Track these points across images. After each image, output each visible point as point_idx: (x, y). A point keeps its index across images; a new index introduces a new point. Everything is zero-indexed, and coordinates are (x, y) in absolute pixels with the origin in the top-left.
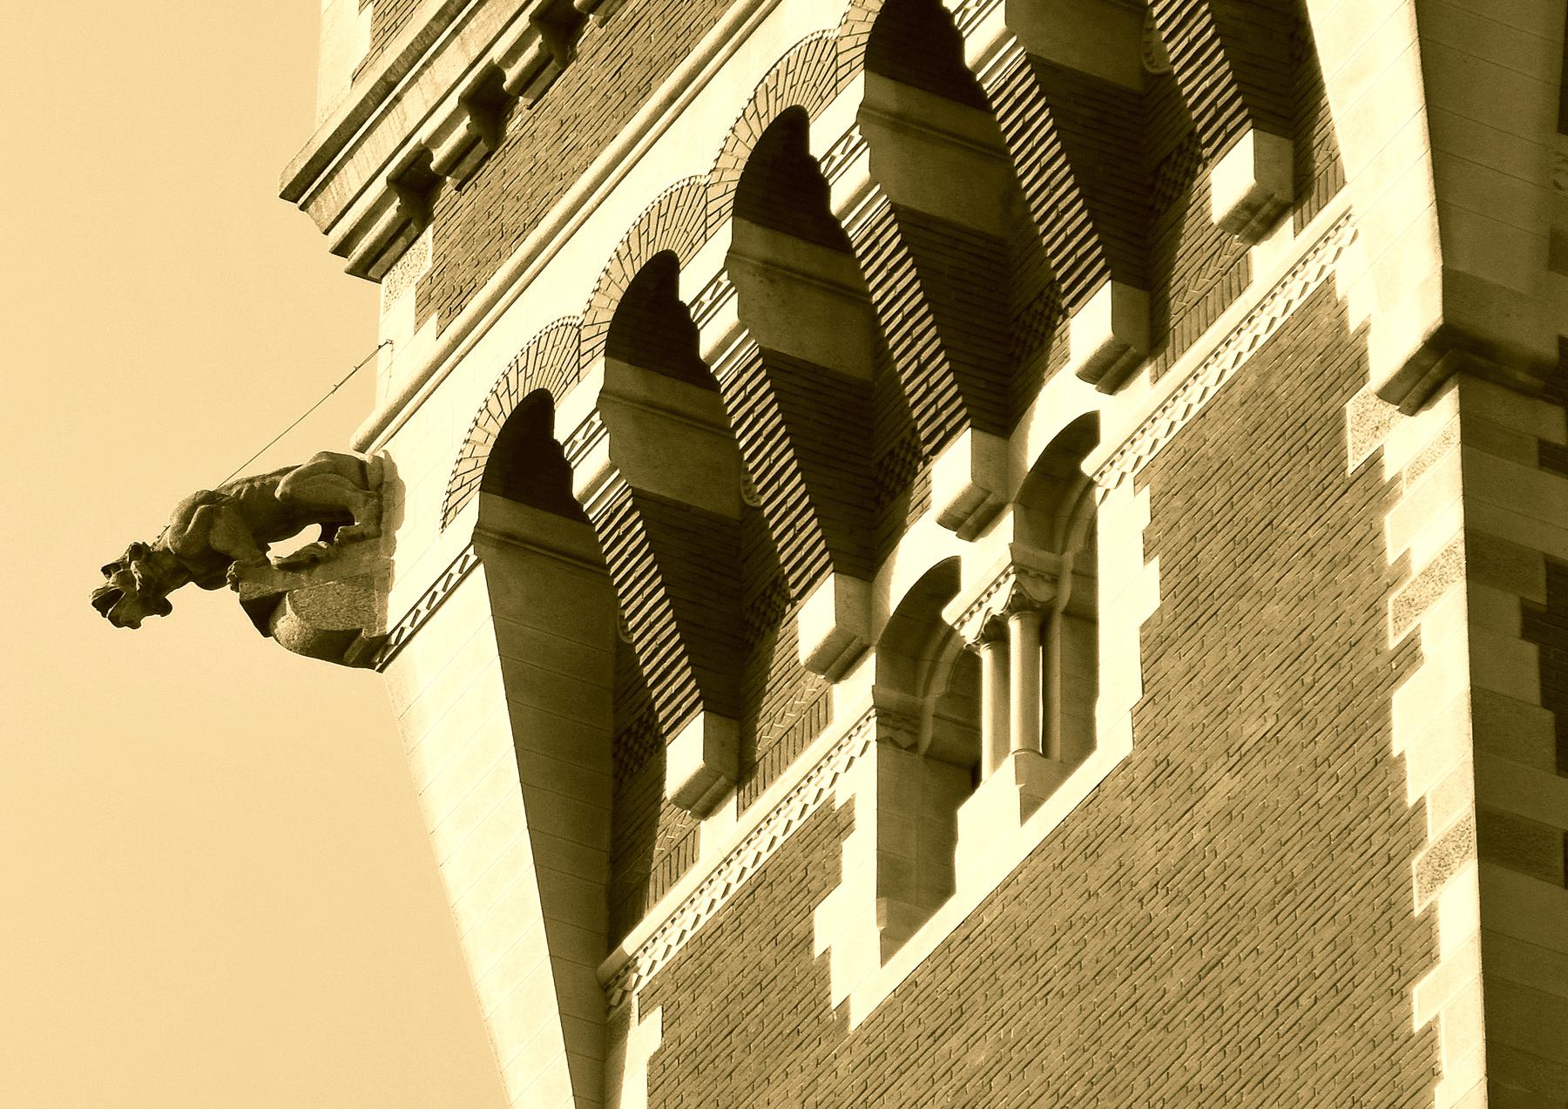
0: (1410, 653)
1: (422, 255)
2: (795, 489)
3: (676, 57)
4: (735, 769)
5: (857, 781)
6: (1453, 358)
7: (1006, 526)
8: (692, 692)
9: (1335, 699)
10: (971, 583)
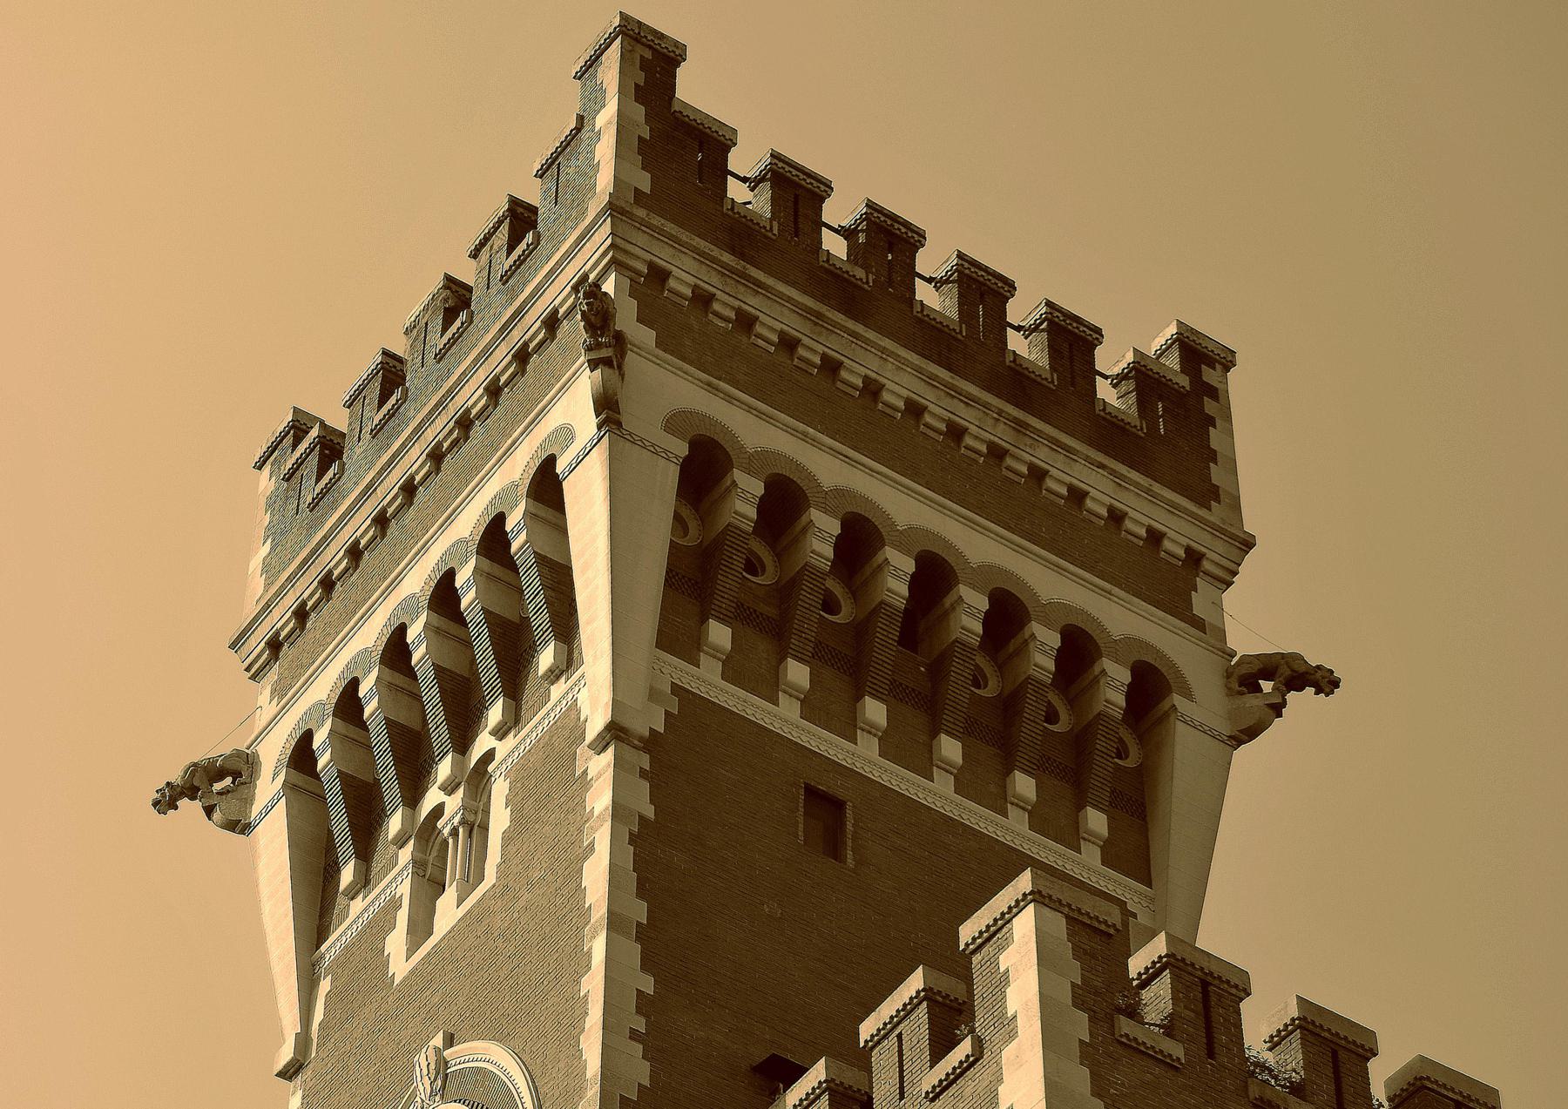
0: (591, 848)
1: (273, 675)
2: (392, 772)
3: (366, 601)
4: (364, 881)
5: (404, 889)
6: (615, 732)
7: (460, 792)
8: (351, 850)
9: (565, 864)
10: (498, 757)
